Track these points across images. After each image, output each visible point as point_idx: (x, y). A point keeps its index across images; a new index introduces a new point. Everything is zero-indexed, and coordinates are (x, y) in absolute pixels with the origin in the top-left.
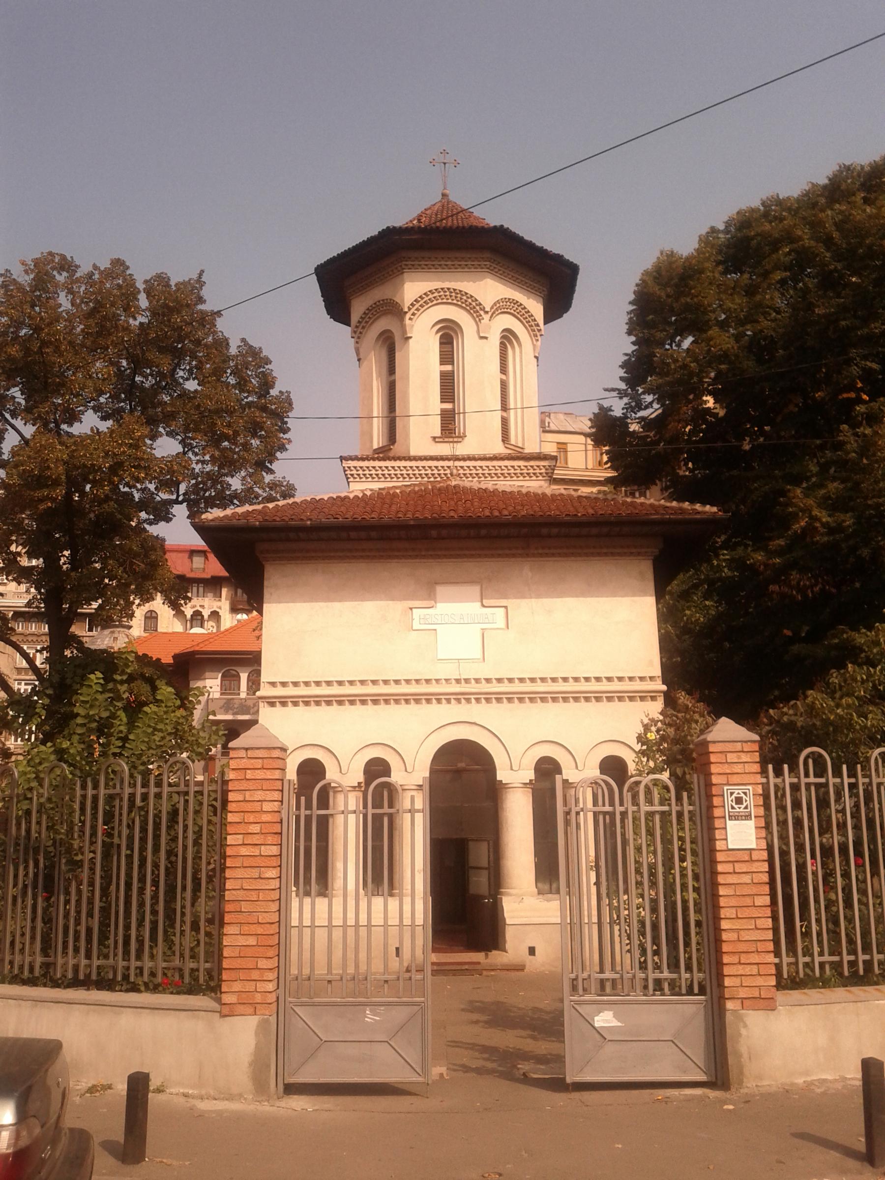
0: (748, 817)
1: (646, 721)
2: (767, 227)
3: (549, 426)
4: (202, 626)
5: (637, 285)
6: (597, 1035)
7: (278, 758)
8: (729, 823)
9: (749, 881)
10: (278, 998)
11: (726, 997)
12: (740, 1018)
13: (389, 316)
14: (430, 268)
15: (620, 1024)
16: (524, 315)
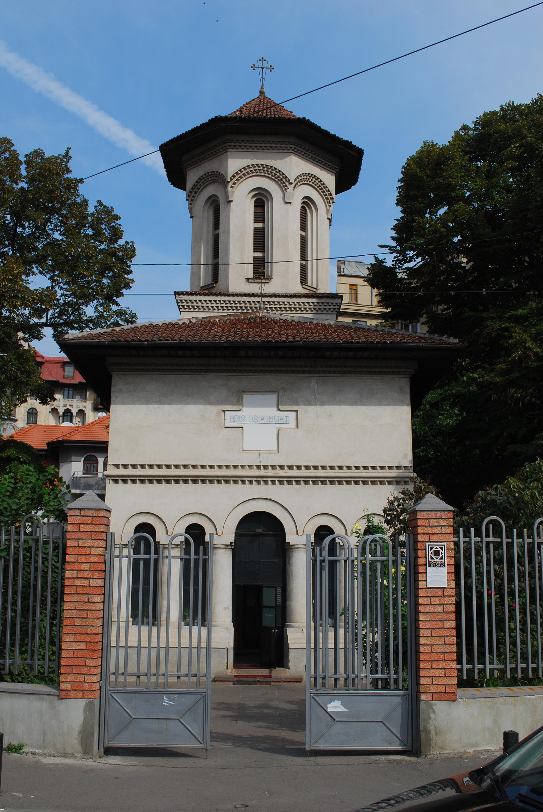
0: (443, 565)
1: (391, 498)
2: (502, 126)
3: (343, 272)
4: (71, 421)
5: (403, 167)
6: (329, 717)
7: (104, 517)
8: (429, 569)
9: (441, 611)
10: (101, 687)
11: (421, 691)
12: (431, 707)
13: (216, 184)
14: (248, 149)
15: (345, 710)
16: (320, 186)
